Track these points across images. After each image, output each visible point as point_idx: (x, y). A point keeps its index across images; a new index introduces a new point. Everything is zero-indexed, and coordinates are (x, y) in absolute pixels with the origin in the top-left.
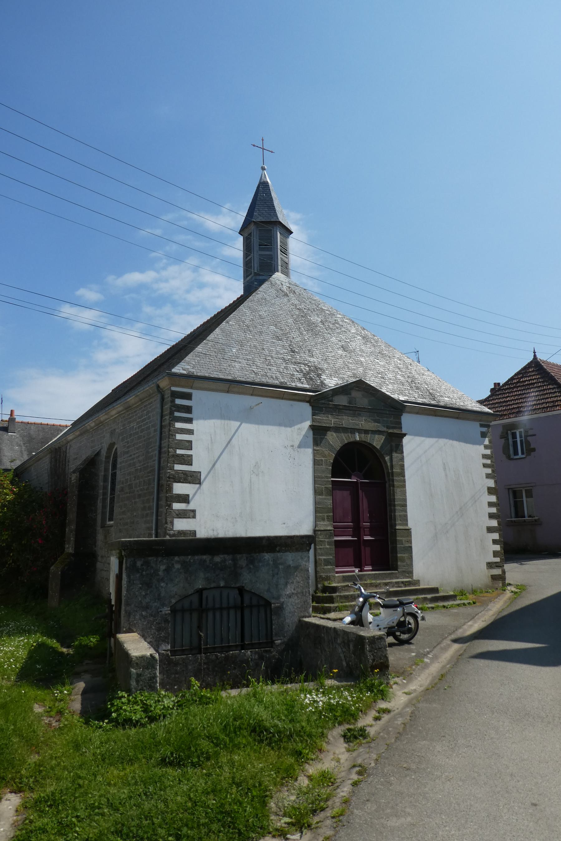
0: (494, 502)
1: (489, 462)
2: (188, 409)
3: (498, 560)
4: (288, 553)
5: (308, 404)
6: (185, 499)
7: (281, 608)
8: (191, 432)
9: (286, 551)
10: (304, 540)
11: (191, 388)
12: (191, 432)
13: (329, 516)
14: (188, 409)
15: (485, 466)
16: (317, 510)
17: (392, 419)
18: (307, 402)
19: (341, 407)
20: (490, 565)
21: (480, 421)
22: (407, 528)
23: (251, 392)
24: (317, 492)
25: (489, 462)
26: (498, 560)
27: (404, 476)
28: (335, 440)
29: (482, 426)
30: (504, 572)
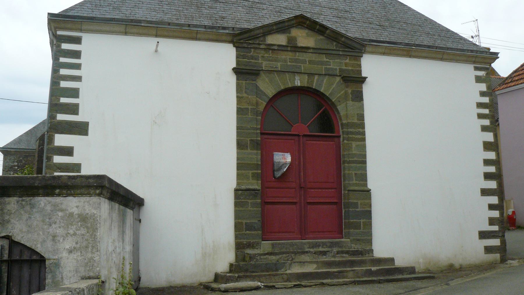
0: (492, 160)
1: (486, 111)
2: (77, 54)
3: (496, 228)
4: (70, 198)
5: (231, 46)
6: (68, 151)
7: (57, 265)
8: (78, 79)
9: (68, 195)
10: (91, 181)
11: (81, 30)
12: (78, 79)
13: (257, 173)
14: (77, 54)
15: (481, 116)
16: (240, 166)
17: (347, 61)
18: (230, 42)
19: (276, 48)
20: (483, 235)
21: (474, 62)
22: (365, 189)
23: (154, 33)
24: (240, 145)
25: (486, 111)
26: (496, 228)
27: (363, 127)
28: (268, 87)
29: (476, 69)
30: (503, 242)
